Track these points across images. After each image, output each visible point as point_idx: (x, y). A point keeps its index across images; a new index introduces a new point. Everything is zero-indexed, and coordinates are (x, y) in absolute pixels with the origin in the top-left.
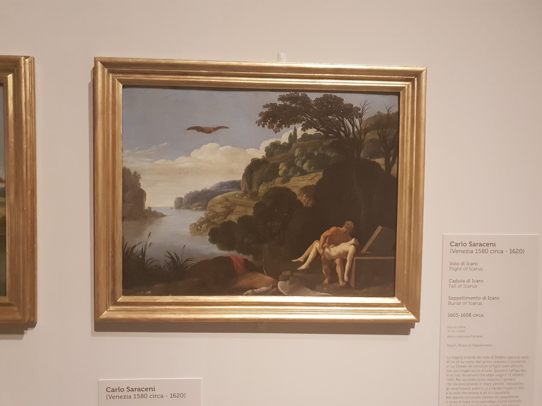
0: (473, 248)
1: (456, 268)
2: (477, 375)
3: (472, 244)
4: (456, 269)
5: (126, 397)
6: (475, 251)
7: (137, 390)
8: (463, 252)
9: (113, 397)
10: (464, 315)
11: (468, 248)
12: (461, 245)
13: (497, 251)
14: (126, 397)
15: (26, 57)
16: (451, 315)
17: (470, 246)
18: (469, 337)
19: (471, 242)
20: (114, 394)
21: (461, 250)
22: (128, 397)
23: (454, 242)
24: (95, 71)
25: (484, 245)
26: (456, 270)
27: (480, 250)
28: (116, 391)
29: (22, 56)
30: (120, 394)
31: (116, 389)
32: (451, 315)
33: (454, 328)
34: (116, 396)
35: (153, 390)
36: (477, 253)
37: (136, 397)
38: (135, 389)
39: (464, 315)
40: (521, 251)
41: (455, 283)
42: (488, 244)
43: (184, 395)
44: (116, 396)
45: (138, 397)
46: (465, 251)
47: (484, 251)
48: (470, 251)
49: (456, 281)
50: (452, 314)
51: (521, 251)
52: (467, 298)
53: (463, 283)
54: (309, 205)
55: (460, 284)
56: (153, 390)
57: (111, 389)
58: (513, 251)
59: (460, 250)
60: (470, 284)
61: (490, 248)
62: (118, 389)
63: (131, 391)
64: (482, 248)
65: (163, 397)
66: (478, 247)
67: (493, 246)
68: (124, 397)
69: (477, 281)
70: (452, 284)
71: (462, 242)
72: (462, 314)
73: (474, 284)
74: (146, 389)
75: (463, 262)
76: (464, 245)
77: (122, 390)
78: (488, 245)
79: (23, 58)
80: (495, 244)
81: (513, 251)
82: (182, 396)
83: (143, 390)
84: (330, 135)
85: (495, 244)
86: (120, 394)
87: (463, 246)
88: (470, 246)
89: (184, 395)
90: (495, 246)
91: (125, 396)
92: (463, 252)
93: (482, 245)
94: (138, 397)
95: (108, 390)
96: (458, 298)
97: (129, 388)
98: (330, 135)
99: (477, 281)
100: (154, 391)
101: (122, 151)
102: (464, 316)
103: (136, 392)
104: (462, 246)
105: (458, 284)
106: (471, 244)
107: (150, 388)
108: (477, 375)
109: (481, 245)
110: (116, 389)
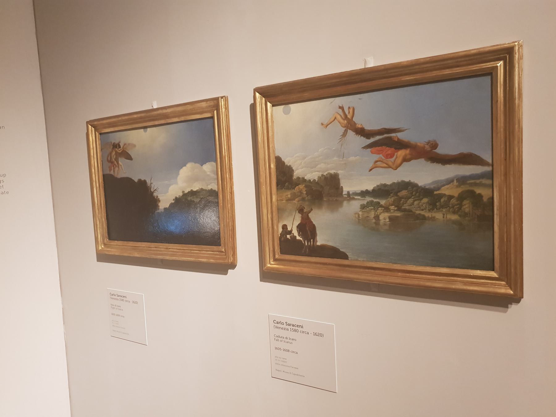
5: (285, 329)
10: (284, 350)
11: (285, 326)
14: (285, 329)
15: (222, 97)
16: (276, 348)
29: (219, 97)
30: (282, 326)
31: (279, 322)
39: (284, 350)
40: (321, 335)
41: (278, 338)
43: (323, 335)
47: (295, 331)
51: (321, 335)
53: (283, 339)
55: (281, 339)
58: (315, 334)
60: (288, 340)
61: (300, 329)
64: (294, 328)
66: (292, 327)
69: (293, 340)
70: (277, 338)
73: (291, 341)
77: (283, 324)
79: (220, 98)
81: (315, 334)
82: (321, 335)
86: (282, 326)
89: (323, 335)
99: (293, 340)
101: (342, 145)
105: (280, 339)
109: (293, 326)
110: (279, 322)
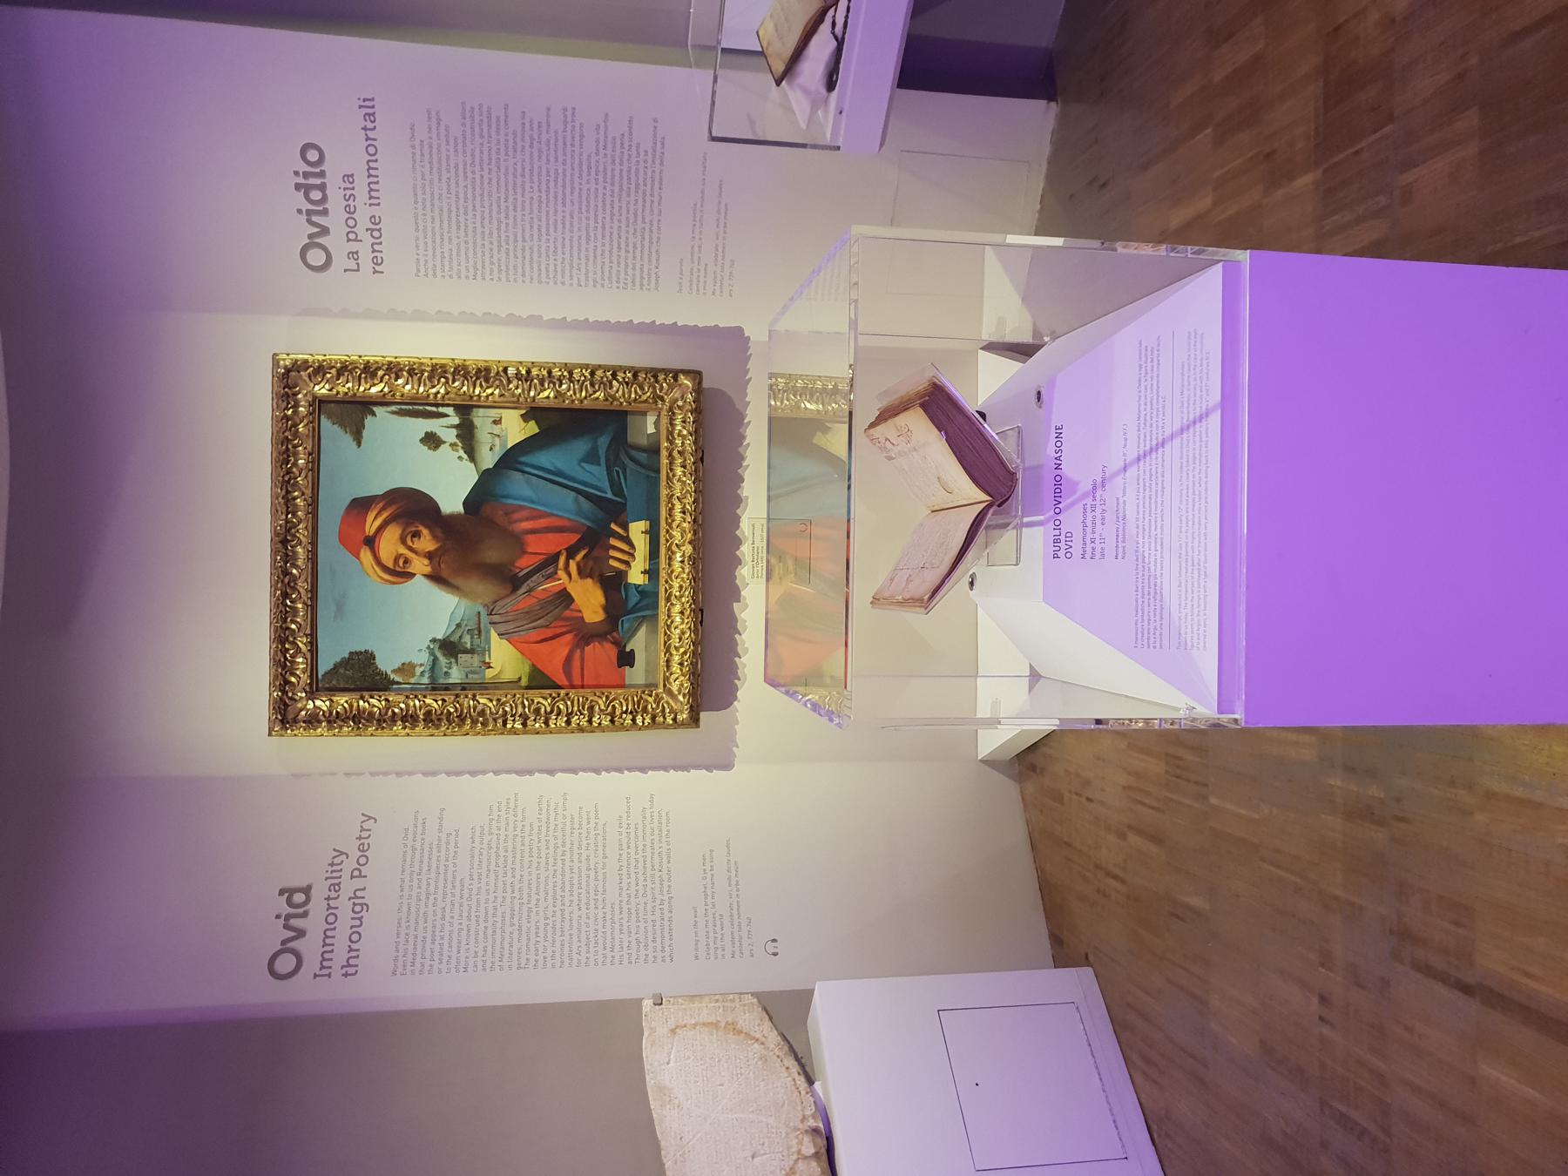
1: (354, 904)
2: (439, 146)
4: (358, 908)
5: (348, 192)
13: (377, 268)
18: (655, 127)
21: (372, 245)
22: (351, 186)
26: (361, 905)
33: (539, 827)
46: (349, 206)
52: (373, 194)
54: (301, 409)
59: (346, 238)
65: (352, 175)
75: (298, 187)
87: (351, 931)
90: (373, 99)
96: (352, 236)
106: (349, 197)
108: (439, 146)
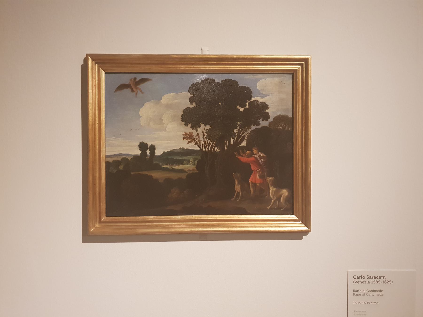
0: (370, 280)
3: (369, 277)
5: (366, 282)
6: (371, 282)
7: (373, 278)
8: (363, 282)
9: (357, 282)
10: (364, 303)
11: (366, 280)
12: (361, 278)
14: (366, 282)
16: (355, 303)
17: (367, 278)
19: (368, 276)
20: (359, 280)
23: (356, 276)
24: (84, 68)
25: (377, 278)
27: (374, 281)
28: (360, 278)
30: (362, 280)
31: (360, 277)
32: (355, 303)
34: (360, 282)
35: (384, 278)
36: (372, 283)
37: (373, 282)
38: (372, 277)
39: (364, 303)
42: (380, 277)
44: (360, 282)
45: (374, 283)
47: (377, 282)
48: (368, 282)
49: (380, 291)
50: (356, 302)
56: (384, 278)
57: (357, 276)
62: (361, 277)
63: (370, 278)
64: (376, 280)
67: (384, 278)
68: (365, 282)
71: (361, 276)
72: (363, 302)
74: (379, 277)
76: (363, 278)
77: (364, 278)
78: (380, 278)
80: (385, 277)
83: (377, 278)
84: (226, 149)
85: (385, 277)
86: (362, 280)
88: (367, 278)
91: (366, 282)
92: (363, 282)
93: (376, 278)
94: (374, 283)
95: (354, 277)
97: (368, 276)
98: (226, 149)
100: (385, 278)
102: (356, 303)
103: (373, 280)
104: (362, 278)
107: (382, 277)
110: (360, 277)
